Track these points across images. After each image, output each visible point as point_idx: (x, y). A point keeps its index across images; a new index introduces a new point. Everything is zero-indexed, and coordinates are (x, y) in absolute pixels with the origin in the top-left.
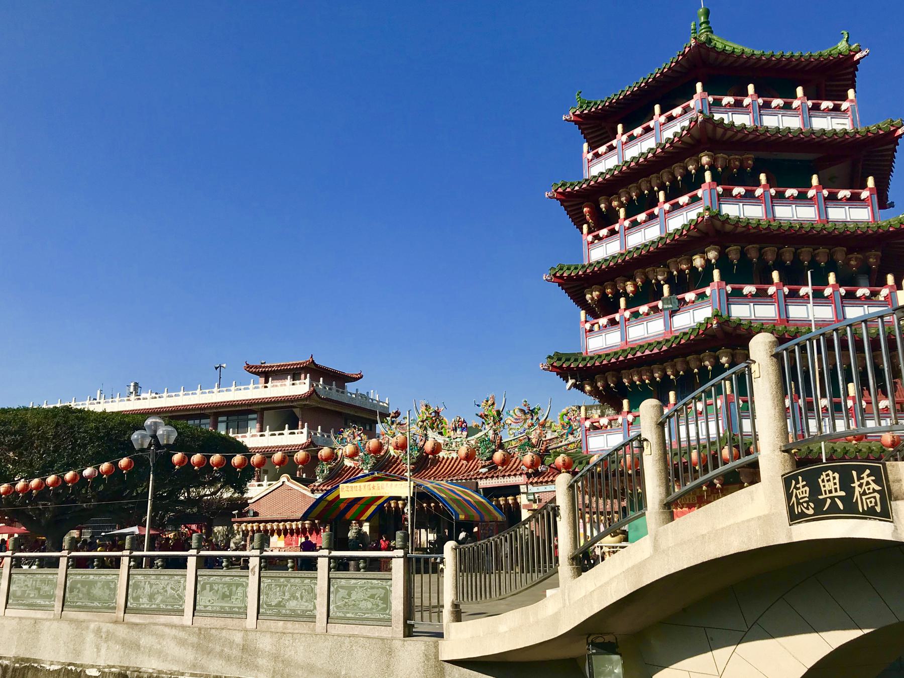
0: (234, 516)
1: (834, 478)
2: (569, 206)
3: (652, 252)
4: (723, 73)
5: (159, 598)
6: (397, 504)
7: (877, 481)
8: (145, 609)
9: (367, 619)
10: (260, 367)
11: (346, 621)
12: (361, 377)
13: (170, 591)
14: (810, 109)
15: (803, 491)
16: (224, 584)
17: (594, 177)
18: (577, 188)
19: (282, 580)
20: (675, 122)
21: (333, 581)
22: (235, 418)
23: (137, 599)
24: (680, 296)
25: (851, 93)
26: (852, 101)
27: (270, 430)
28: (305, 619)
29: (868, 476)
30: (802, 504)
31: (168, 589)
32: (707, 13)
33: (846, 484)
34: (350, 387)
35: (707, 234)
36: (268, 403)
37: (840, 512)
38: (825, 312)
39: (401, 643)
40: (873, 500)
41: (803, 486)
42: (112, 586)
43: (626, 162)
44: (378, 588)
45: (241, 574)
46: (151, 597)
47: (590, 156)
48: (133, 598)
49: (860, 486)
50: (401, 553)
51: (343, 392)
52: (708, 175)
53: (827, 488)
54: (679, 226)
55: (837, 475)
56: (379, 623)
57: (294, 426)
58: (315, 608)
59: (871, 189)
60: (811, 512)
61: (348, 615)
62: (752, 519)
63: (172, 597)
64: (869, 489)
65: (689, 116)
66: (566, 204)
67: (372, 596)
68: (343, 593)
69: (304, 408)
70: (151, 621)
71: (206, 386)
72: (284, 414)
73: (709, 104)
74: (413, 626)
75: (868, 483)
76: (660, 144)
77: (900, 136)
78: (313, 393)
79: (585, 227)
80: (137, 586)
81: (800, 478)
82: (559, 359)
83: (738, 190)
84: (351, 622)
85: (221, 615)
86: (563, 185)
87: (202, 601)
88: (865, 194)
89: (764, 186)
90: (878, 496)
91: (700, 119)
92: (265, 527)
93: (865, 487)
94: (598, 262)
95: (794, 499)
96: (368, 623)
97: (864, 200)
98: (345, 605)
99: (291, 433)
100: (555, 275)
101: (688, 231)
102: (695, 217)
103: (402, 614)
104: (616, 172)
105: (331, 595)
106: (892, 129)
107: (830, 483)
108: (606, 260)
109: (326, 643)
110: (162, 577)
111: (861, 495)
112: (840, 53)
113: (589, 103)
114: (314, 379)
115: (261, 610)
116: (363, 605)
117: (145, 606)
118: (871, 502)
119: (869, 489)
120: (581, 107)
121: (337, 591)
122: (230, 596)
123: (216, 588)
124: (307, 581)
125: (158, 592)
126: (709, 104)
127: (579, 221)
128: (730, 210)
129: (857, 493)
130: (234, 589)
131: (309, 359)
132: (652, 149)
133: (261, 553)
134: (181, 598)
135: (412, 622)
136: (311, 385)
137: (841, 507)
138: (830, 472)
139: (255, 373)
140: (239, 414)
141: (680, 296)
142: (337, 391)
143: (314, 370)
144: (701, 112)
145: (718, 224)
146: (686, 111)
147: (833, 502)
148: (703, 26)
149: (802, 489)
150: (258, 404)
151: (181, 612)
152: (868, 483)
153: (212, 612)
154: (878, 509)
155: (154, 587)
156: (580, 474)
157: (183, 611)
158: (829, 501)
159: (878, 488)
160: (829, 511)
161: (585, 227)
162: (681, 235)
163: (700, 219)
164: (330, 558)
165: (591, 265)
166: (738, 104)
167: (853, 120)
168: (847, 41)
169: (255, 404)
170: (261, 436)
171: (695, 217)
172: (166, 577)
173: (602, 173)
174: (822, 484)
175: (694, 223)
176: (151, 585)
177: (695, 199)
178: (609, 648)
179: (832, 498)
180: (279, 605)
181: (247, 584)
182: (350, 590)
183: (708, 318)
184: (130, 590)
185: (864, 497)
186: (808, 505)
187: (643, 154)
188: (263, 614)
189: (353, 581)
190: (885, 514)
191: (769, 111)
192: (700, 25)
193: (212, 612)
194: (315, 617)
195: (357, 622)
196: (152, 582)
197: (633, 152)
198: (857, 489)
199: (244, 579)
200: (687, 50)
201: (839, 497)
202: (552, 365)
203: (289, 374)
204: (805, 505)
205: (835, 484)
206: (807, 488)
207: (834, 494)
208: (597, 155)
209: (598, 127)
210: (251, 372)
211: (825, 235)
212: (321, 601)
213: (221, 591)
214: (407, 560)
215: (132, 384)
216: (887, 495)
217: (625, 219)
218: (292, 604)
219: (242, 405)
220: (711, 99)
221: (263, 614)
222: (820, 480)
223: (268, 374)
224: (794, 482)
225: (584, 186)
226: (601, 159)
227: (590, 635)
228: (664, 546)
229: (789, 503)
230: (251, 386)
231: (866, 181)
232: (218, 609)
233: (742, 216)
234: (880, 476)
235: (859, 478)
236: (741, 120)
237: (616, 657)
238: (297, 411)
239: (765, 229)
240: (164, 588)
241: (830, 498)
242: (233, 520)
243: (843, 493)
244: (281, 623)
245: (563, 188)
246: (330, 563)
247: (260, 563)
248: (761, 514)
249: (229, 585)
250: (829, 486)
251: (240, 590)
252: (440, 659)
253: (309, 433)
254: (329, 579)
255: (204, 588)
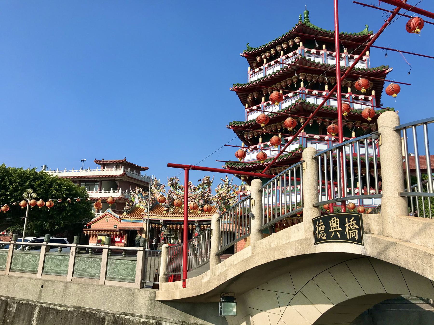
0: (84, 228)
1: (337, 221)
2: (241, 95)
3: (274, 118)
4: (312, 38)
5: (26, 265)
6: (192, 227)
7: (357, 224)
8: (19, 270)
9: (124, 279)
10: (102, 161)
11: (114, 280)
12: (147, 169)
13: (32, 262)
14: (349, 58)
15: (322, 228)
16: (58, 259)
17: (252, 82)
18: (244, 87)
19: (86, 258)
20: (289, 59)
21: (109, 260)
22: (89, 184)
23: (16, 265)
24: (286, 138)
25: (367, 53)
26: (368, 56)
27: (104, 190)
28: (95, 278)
29: (353, 221)
30: (321, 234)
31: (31, 260)
32: (308, 13)
33: (342, 224)
34: (142, 173)
35: (299, 111)
36: (104, 178)
37: (338, 239)
38: (319, 101)
39: (138, 291)
40: (354, 233)
41: (322, 225)
42: (5, 258)
43: (266, 76)
44: (130, 264)
45: (67, 255)
46: (23, 264)
47: (251, 73)
48: (14, 264)
49: (349, 226)
50: (142, 248)
51: (139, 175)
52: (302, 84)
53: (333, 226)
54: (287, 107)
55: (338, 220)
56: (129, 281)
57: (115, 189)
58: (100, 272)
59: (373, 96)
60: (325, 238)
61: (115, 277)
62: (295, 241)
63: (33, 265)
64: (353, 227)
65: (295, 57)
66: (239, 94)
67: (127, 268)
68: (113, 266)
69: (120, 181)
70: (22, 275)
71: (76, 168)
72: (111, 183)
73: (305, 52)
74: (145, 283)
75: (353, 224)
76: (282, 68)
77: (387, 73)
78: (125, 174)
79: (247, 105)
80: (16, 259)
81: (321, 220)
82: (231, 164)
83: (315, 92)
84: (116, 280)
85: (55, 274)
86: (238, 85)
87: (47, 267)
88: (370, 98)
89: (327, 91)
90: (357, 231)
91: (300, 58)
92: (116, 233)
93: (351, 226)
94: (251, 121)
95: (317, 231)
96: (124, 281)
97: (370, 101)
98: (114, 272)
99: (113, 192)
100: (231, 126)
101: (291, 108)
102: (294, 103)
103: (140, 277)
104: (261, 80)
105: (108, 267)
106: (384, 69)
107: (335, 224)
108: (254, 120)
109: (103, 290)
110: (28, 255)
111: (349, 230)
112: (364, 34)
113: (252, 49)
114: (126, 168)
115: (74, 273)
116: (123, 272)
117: (19, 268)
118: (353, 234)
119: (353, 227)
120: (248, 50)
121: (111, 265)
122: (60, 265)
123: (54, 261)
124: (97, 259)
125: (26, 262)
126: (305, 52)
127: (244, 102)
128: (311, 100)
129: (347, 229)
130: (62, 262)
131: (123, 159)
132: (278, 71)
133: (77, 245)
134: (37, 265)
135: (145, 281)
136: (124, 171)
137: (339, 236)
138: (335, 218)
139: (99, 164)
140: (91, 182)
141: (286, 138)
142: (136, 174)
143: (126, 164)
144: (301, 55)
145: (304, 106)
146: (295, 54)
147: (336, 234)
148: (306, 19)
149: (321, 226)
150: (99, 178)
151: (36, 272)
152: (353, 224)
153: (51, 272)
154: (357, 238)
155: (24, 259)
156: (373, 236)
157: (37, 271)
158: (334, 233)
159: (357, 227)
160: (333, 238)
161: (247, 105)
162: (288, 110)
163: (297, 103)
164: (109, 249)
165: (247, 122)
166: (318, 53)
167: (367, 65)
168: (367, 29)
169: (98, 178)
170: (100, 192)
171: (294, 103)
172: (30, 255)
173: (255, 81)
174: (331, 224)
175: (294, 105)
176: (23, 259)
177: (295, 95)
178: (231, 299)
179: (335, 231)
180: (83, 270)
181: (69, 260)
182: (117, 264)
183: (297, 148)
184: (13, 260)
185: (350, 232)
186: (324, 234)
187: (274, 72)
188: (75, 274)
189: (119, 261)
190: (360, 241)
191: (331, 57)
192: (305, 18)
193: (51, 272)
194: (99, 277)
195: (119, 280)
196: (24, 257)
197: (270, 72)
198: (348, 227)
199: (68, 257)
200: (297, 27)
201: (338, 231)
202: (227, 166)
203: (114, 165)
204: (322, 234)
205: (337, 224)
206: (324, 226)
207: (336, 229)
208: (254, 73)
209: (253, 59)
210: (97, 163)
211: (352, 115)
212: (103, 270)
213: (56, 262)
214: (145, 252)
215: (44, 166)
216: (361, 231)
217: (264, 102)
218: (90, 270)
219: (92, 178)
220: (306, 50)
221: (75, 274)
222: (330, 222)
223: (104, 164)
224: (318, 222)
225: (247, 86)
226: (256, 74)
227: (222, 293)
228: (256, 251)
229: (315, 233)
230: (97, 170)
231: (371, 93)
232: (54, 271)
233: (316, 104)
234: (359, 221)
235: (349, 222)
236: (318, 60)
237: (233, 304)
238: (117, 183)
239: (326, 110)
240: (29, 260)
241: (334, 231)
242: (84, 229)
243: (340, 229)
244: (83, 279)
245: (238, 86)
246: (108, 252)
247: (76, 250)
248: (302, 238)
249: (61, 260)
250: (334, 225)
251: (65, 262)
252: (156, 299)
253: (122, 192)
254: (108, 259)
255: (48, 261)
